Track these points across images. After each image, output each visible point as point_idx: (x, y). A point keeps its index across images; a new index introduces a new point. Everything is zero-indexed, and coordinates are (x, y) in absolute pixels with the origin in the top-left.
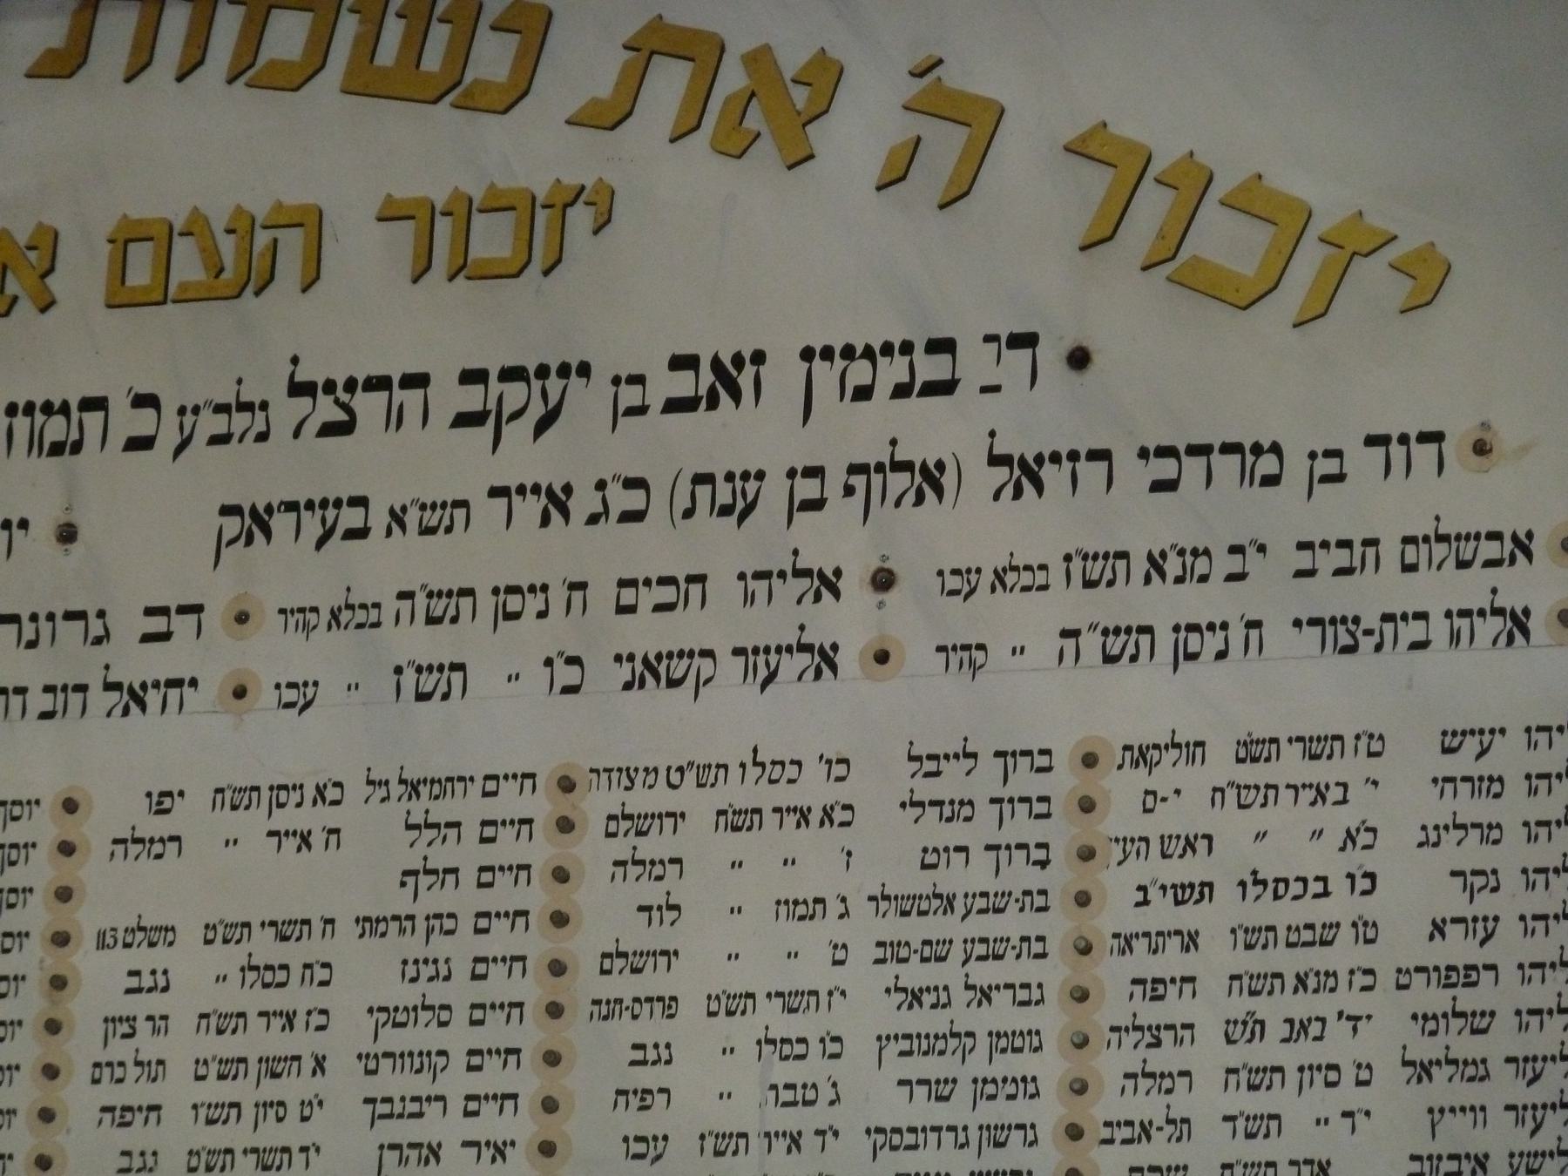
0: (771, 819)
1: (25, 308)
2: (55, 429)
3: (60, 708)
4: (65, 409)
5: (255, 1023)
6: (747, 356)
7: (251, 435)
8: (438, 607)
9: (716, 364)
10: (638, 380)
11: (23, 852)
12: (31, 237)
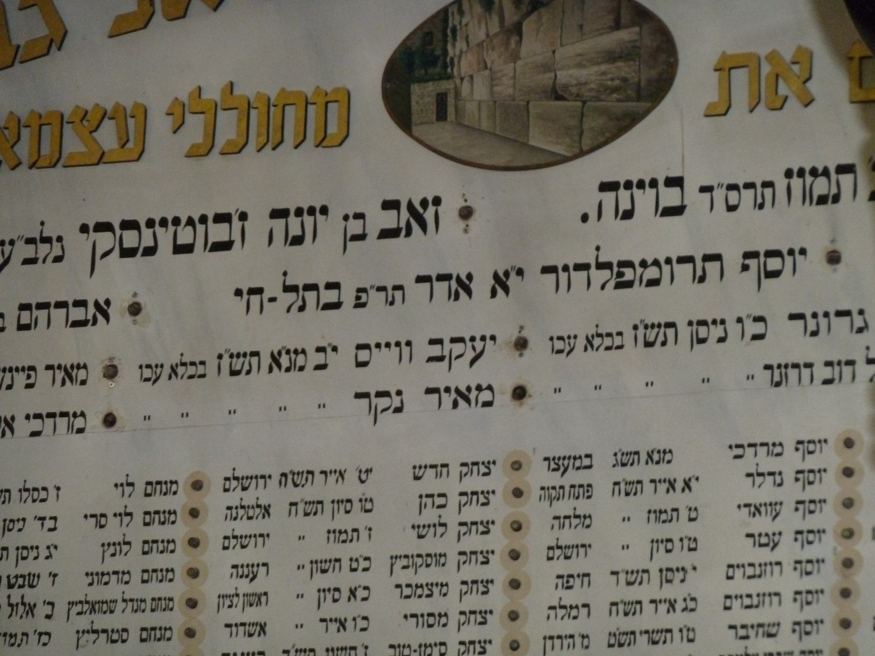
0: (648, 487)
1: (793, 104)
2: (821, 186)
3: (837, 377)
4: (826, 173)
5: (648, 608)
6: (430, 200)
7: (50, 259)
8: (237, 364)
9: (411, 207)
10: (359, 216)
11: (818, 475)
12: (793, 57)
